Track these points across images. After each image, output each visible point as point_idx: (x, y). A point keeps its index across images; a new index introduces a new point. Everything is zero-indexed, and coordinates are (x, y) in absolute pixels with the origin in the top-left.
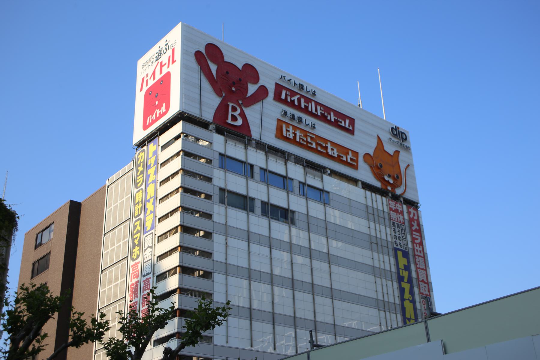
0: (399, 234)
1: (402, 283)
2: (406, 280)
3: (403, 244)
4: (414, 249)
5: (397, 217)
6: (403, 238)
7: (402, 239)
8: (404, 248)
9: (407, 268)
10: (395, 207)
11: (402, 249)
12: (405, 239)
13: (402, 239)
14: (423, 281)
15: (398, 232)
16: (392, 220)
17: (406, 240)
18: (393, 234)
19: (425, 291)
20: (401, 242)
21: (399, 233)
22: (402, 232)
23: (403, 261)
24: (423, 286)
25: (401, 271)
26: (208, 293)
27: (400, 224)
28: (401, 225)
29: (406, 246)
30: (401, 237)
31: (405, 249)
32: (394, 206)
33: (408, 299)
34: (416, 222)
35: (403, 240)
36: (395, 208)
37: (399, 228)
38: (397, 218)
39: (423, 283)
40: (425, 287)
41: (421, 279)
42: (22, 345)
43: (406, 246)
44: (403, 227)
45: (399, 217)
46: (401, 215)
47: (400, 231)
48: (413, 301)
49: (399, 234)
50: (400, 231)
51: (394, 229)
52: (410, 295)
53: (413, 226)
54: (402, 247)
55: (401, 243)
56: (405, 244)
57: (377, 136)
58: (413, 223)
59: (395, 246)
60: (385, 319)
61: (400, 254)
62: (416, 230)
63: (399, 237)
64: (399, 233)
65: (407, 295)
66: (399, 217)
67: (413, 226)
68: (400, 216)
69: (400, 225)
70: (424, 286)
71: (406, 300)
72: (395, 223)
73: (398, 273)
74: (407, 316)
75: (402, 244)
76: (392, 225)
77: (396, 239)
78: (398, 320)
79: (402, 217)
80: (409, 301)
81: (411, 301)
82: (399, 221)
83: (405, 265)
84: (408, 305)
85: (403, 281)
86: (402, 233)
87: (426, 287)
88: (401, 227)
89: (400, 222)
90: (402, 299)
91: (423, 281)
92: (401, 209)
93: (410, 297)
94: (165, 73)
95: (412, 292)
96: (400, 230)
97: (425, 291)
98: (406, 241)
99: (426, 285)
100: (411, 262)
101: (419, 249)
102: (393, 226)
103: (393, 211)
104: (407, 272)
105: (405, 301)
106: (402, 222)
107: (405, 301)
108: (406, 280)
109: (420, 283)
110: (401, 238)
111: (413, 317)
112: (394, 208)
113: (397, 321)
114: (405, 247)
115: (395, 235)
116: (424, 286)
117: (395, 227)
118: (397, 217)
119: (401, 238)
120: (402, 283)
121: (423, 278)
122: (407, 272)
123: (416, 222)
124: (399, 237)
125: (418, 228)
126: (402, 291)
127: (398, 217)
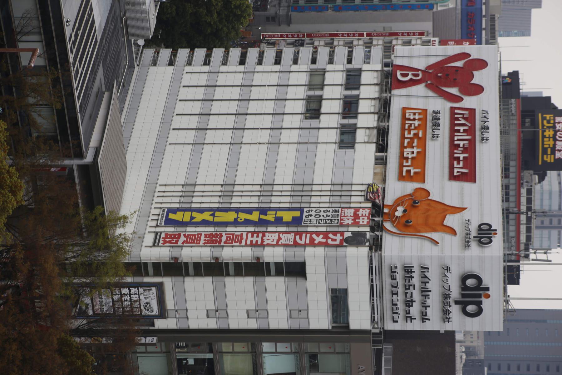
0: (323, 216)
1: (258, 212)
2: (262, 217)
3: (311, 219)
5: (347, 216)
6: (320, 221)
7: (318, 219)
8: (305, 220)
9: (279, 221)
10: (362, 215)
11: (304, 218)
12: (319, 223)
13: (318, 219)
14: (280, 238)
15: (327, 215)
17: (318, 224)
18: (322, 210)
19: (268, 240)
20: (313, 217)
21: (325, 216)
22: (328, 220)
23: (287, 217)
24: (273, 237)
25: (274, 212)
28: (338, 220)
29: (308, 222)
30: (320, 218)
31: (304, 221)
32: (362, 214)
35: (317, 220)
36: (360, 215)
37: (333, 217)
39: (277, 238)
40: (273, 240)
41: (281, 235)
43: (308, 222)
44: (336, 223)
47: (328, 218)
48: (236, 223)
49: (323, 216)
50: (328, 218)
52: (243, 220)
54: (306, 217)
59: (305, 210)
60: (167, 186)
61: (297, 214)
62: (312, 240)
64: (325, 216)
65: (243, 216)
66: (349, 219)
67: (318, 236)
68: (350, 220)
69: (337, 218)
70: (273, 239)
71: (237, 214)
72: (338, 212)
73: (270, 209)
74: (217, 214)
75: (310, 218)
76: (334, 209)
77: (315, 212)
78: (172, 204)
79: (350, 223)
80: (236, 217)
81: (236, 220)
82: (342, 218)
84: (230, 217)
86: (327, 220)
90: (237, 210)
92: (361, 223)
93: (241, 219)
94: (100, 66)
95: (247, 223)
96: (330, 218)
97: (268, 240)
98: (317, 223)
99: (275, 243)
101: (473, 237)
102: (333, 210)
104: (273, 220)
106: (342, 221)
108: (262, 217)
109: (277, 234)
113: (171, 203)
114: (307, 222)
115: (320, 211)
117: (332, 212)
118: (347, 216)
120: (258, 212)
121: (283, 239)
122: (273, 220)
124: (320, 216)
125: (316, 242)
126: (249, 211)
127: (348, 218)
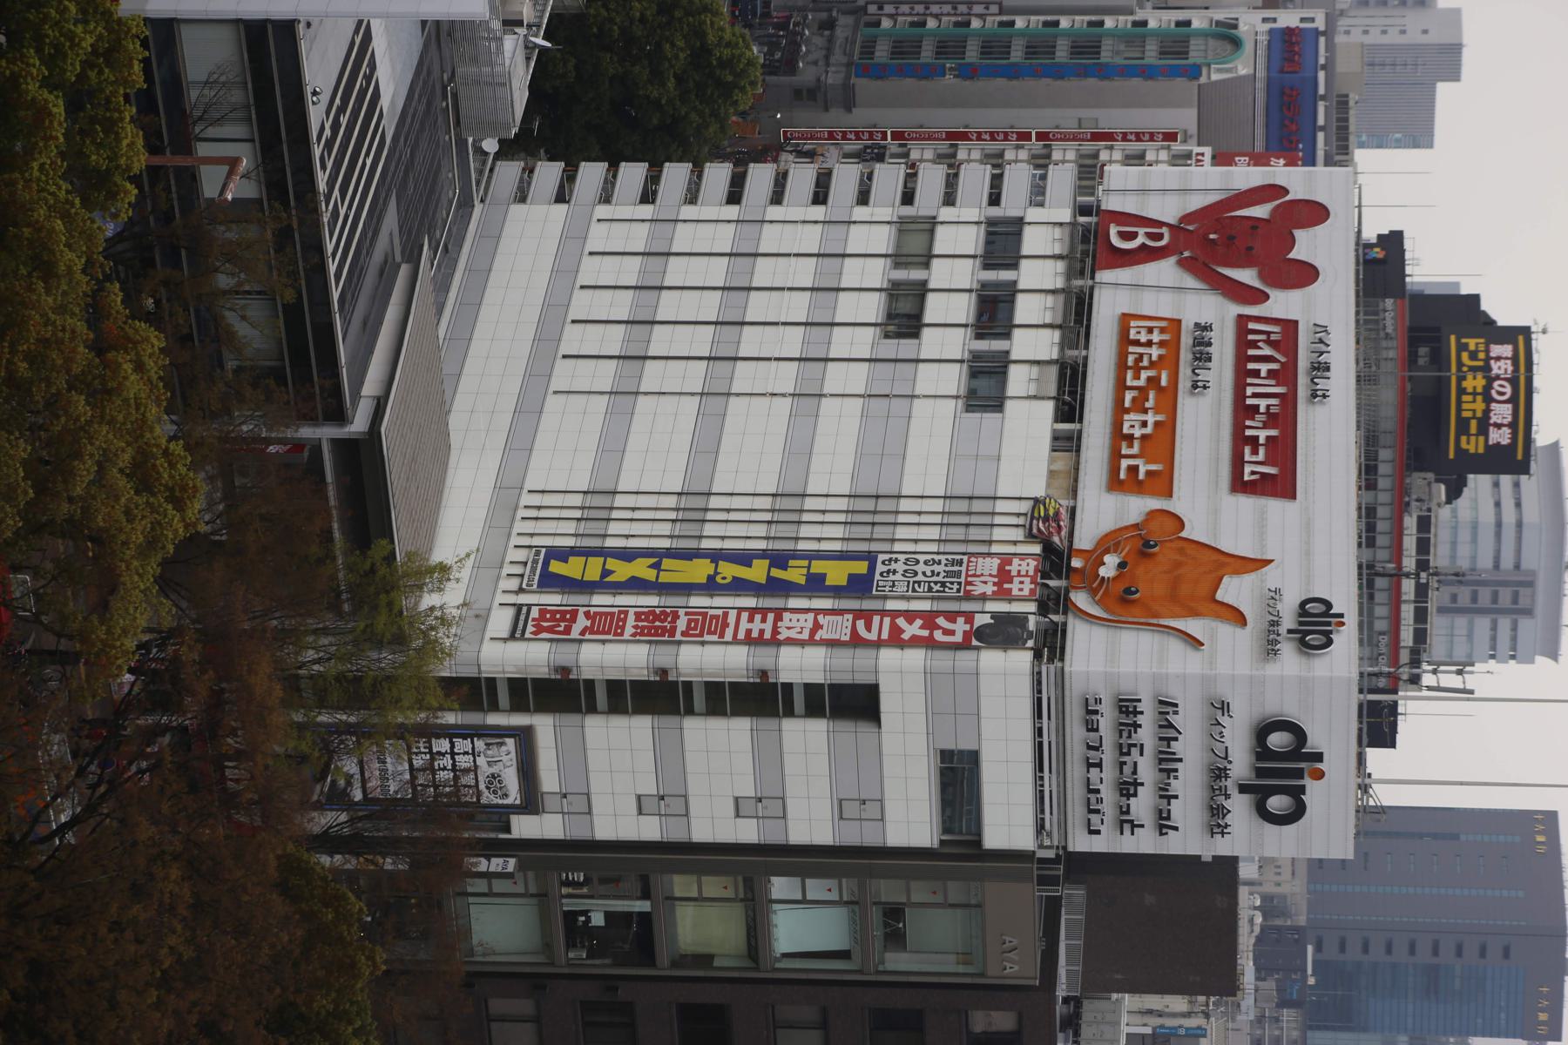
1: (767, 562)
2: (777, 573)
4: (883, 613)
6: (916, 585)
9: (816, 584)
12: (914, 590)
13: (911, 580)
16: (969, 561)
17: (910, 593)
19: (789, 628)
20: (898, 577)
22: (936, 583)
23: (837, 573)
24: (802, 623)
25: (805, 563)
26: (312, 419)
27: (963, 579)
28: (959, 583)
29: (887, 589)
32: (1019, 571)
33: (719, 570)
34: (925, 633)
35: (909, 582)
36: (1014, 573)
38: (978, 573)
41: (820, 618)
42: (241, 333)
43: (887, 589)
44: (955, 590)
45: (985, 583)
46: (995, 588)
48: (711, 586)
50: (935, 579)
51: (940, 561)
53: (910, 622)
55: (894, 574)
56: (894, 586)
57: (1269, 558)
58: (919, 622)
61: (861, 567)
63: (916, 574)
64: (929, 574)
65: (729, 571)
67: (910, 622)
68: (990, 584)
71: (714, 565)
73: (796, 555)
75: (892, 577)
77: (905, 564)
78: (830, 500)
79: (989, 593)
81: (711, 578)
82: (970, 579)
83: (823, 577)
84: (699, 571)
85: (771, 566)
87: (801, 633)
88: (952, 583)
89: (968, 583)
90: (716, 556)
91: (817, 626)
93: (724, 578)
95: (739, 586)
97: (789, 628)
100: (837, 601)
101: (1285, 631)
102: (947, 560)
103: (1001, 569)
104: (802, 581)
105: (712, 562)
106: (968, 588)
107: (712, 562)
108: (777, 573)
110: (915, 579)
111: (665, 578)
112: (1014, 568)
116: (802, 628)
117: (946, 565)
118: (982, 575)
119: (915, 579)
120: (767, 562)
121: (825, 628)
123: (925, 633)
125: (906, 636)
